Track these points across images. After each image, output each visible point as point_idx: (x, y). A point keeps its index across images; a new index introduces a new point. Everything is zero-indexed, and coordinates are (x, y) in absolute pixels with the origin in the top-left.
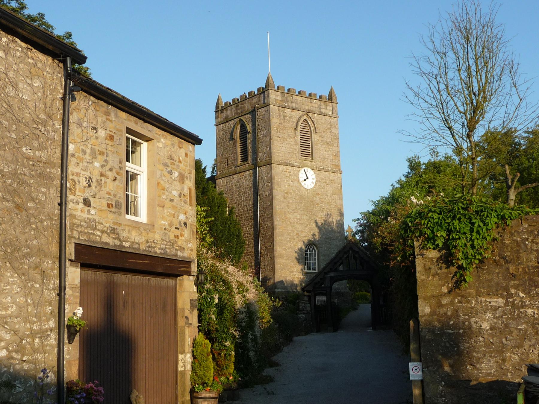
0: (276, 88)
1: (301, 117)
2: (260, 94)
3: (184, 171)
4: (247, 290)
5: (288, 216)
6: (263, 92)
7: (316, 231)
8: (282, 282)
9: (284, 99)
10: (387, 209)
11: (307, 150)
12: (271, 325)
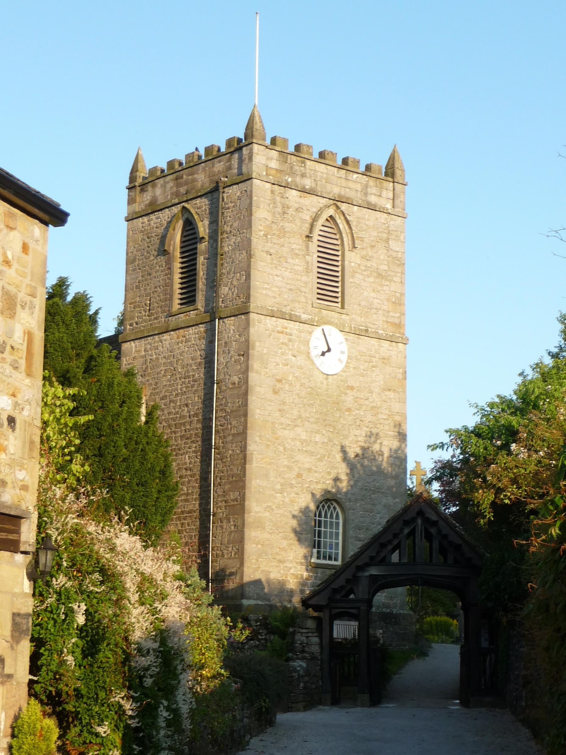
0: (268, 142)
1: (321, 210)
2: (232, 153)
3: (17, 287)
4: (163, 597)
5: (280, 433)
6: (239, 149)
7: (342, 470)
8: (258, 583)
9: (286, 167)
10: (510, 422)
11: (330, 285)
12: (222, 684)
